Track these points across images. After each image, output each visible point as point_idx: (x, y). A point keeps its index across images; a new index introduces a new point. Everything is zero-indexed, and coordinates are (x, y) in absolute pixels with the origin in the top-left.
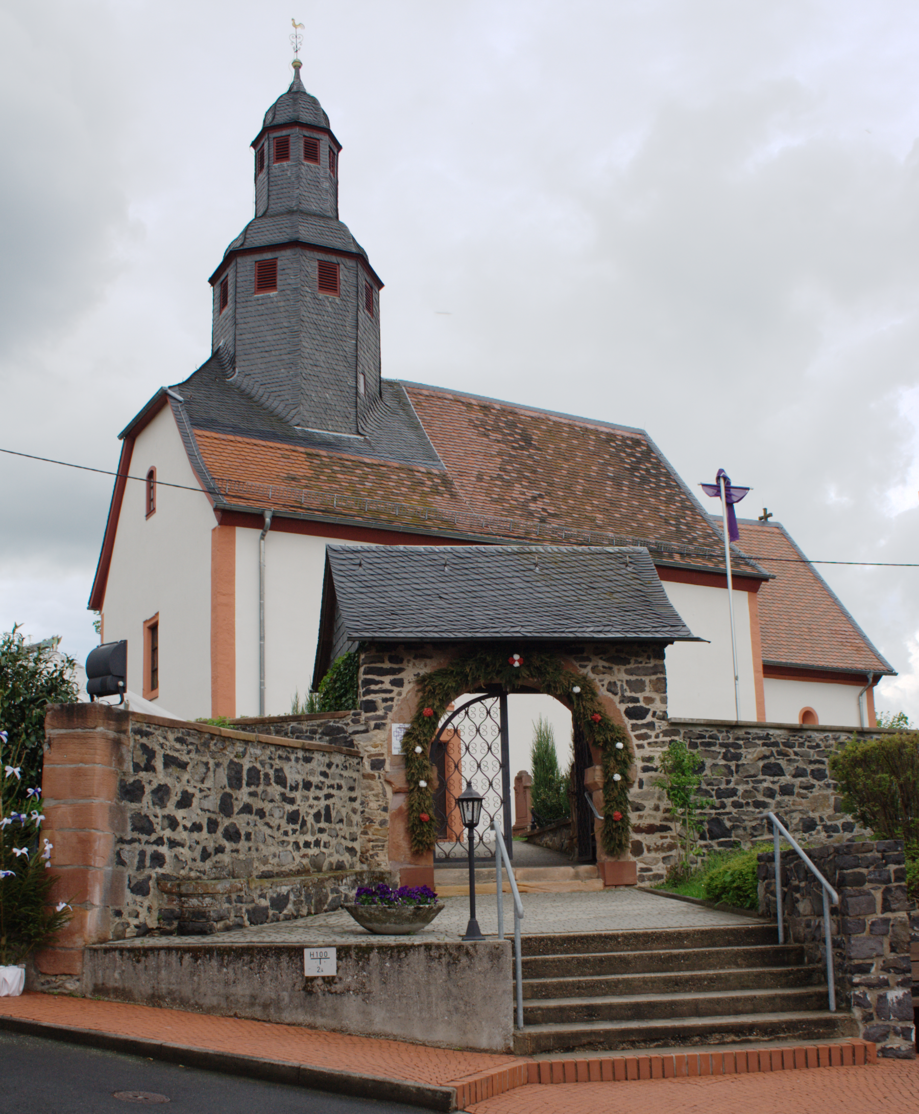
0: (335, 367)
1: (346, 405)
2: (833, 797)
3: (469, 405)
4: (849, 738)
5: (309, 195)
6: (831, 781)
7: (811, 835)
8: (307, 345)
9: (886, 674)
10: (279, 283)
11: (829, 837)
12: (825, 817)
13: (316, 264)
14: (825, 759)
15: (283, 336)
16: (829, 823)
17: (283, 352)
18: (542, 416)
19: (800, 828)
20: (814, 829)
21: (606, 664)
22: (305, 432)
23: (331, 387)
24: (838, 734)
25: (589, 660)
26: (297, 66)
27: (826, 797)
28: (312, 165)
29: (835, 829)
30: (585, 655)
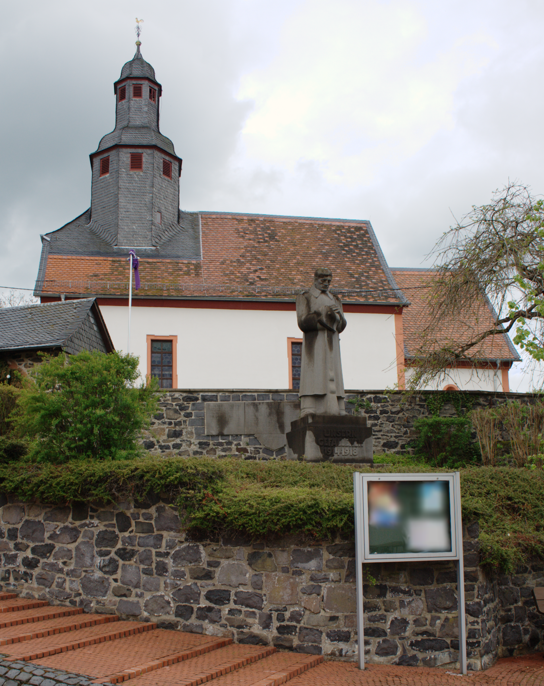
0: (139, 211)
1: (146, 231)
2: (167, 429)
3: (240, 221)
4: (181, 395)
5: (136, 116)
6: (166, 420)
7: (151, 451)
8: (122, 201)
9: (514, 361)
10: (110, 169)
11: (163, 452)
12: (161, 441)
13: (129, 155)
14: (163, 408)
15: (111, 198)
16: (163, 444)
17: (111, 206)
18: (292, 221)
19: (143, 447)
20: (153, 448)
21: (31, 362)
22: (119, 248)
23: (136, 222)
24: (173, 393)
25: (23, 361)
26: (139, 44)
27: (163, 430)
28: (137, 99)
29: (168, 447)
30: (22, 358)
